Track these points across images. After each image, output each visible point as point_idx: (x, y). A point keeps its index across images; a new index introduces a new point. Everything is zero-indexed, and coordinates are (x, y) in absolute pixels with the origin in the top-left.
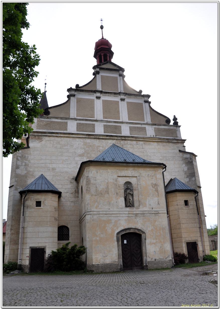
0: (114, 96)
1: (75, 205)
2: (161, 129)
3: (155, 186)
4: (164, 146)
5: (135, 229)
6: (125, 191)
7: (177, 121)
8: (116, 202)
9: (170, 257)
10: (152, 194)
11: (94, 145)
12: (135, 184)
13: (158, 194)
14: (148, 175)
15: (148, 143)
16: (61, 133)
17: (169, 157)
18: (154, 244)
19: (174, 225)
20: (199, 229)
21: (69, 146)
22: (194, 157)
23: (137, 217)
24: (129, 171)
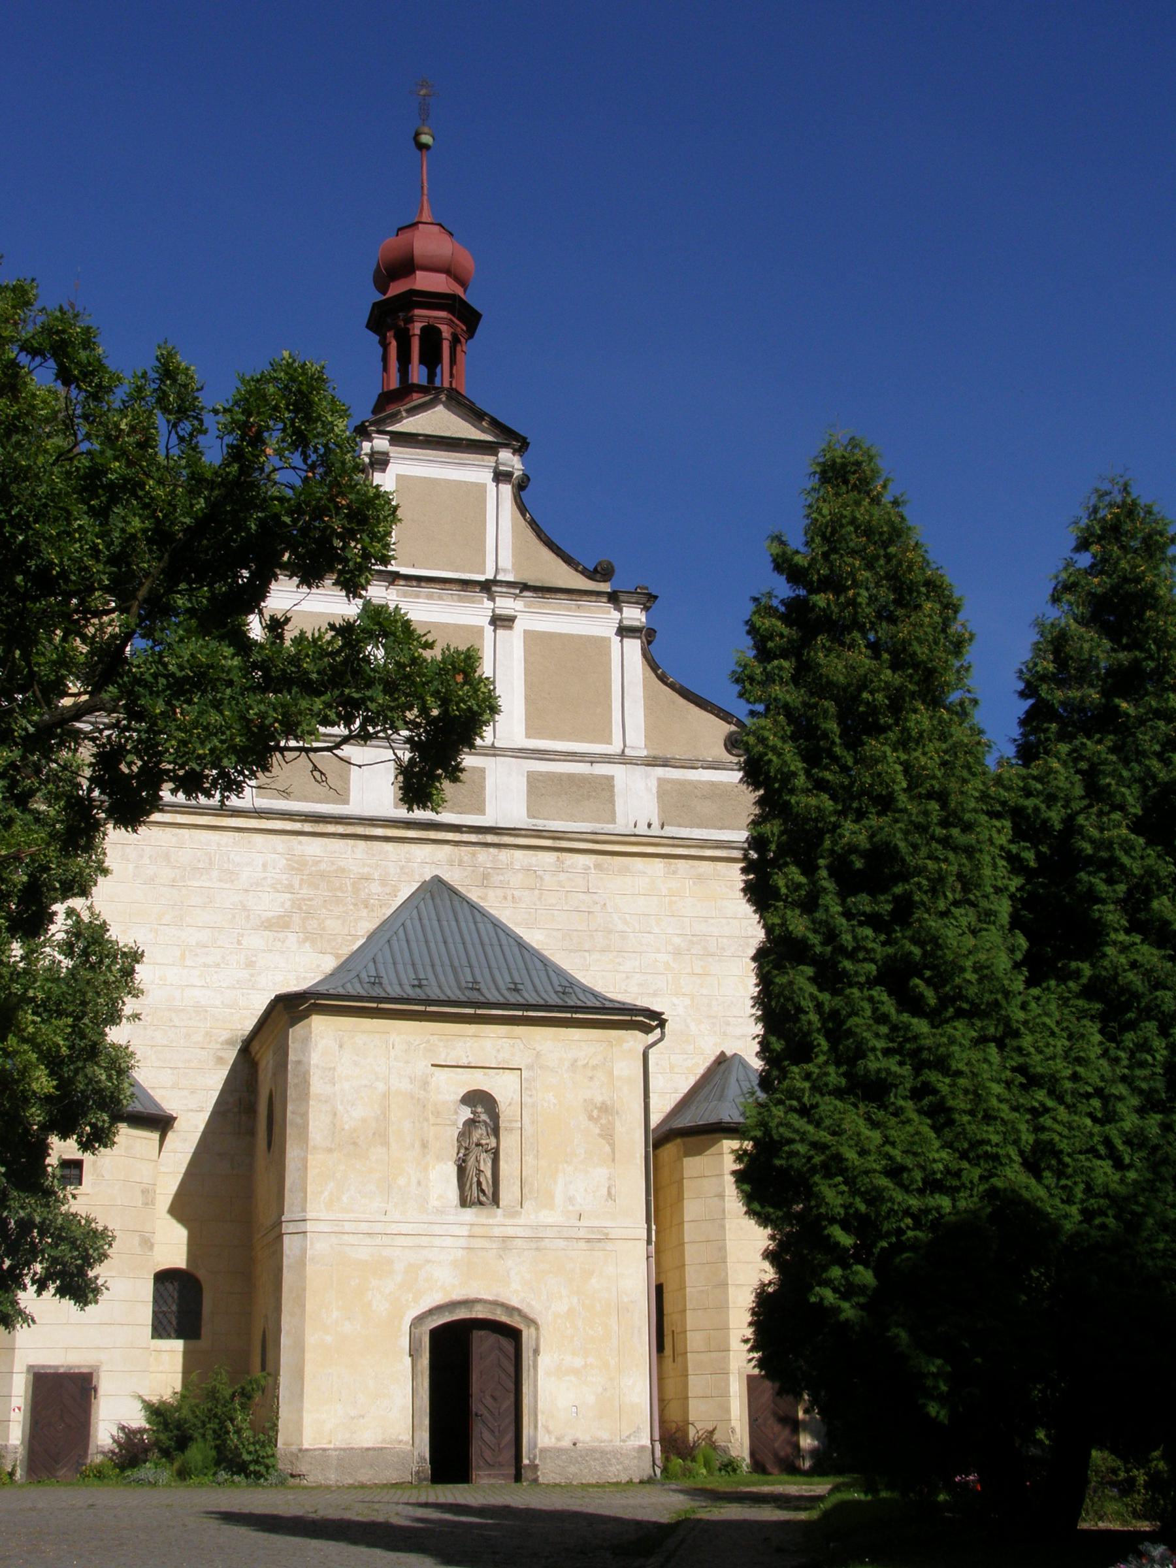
2: (695, 785)
3: (603, 1112)
5: (496, 1303)
8: (419, 1183)
11: (343, 870)
12: (510, 1104)
14: (576, 1061)
21: (215, 874)
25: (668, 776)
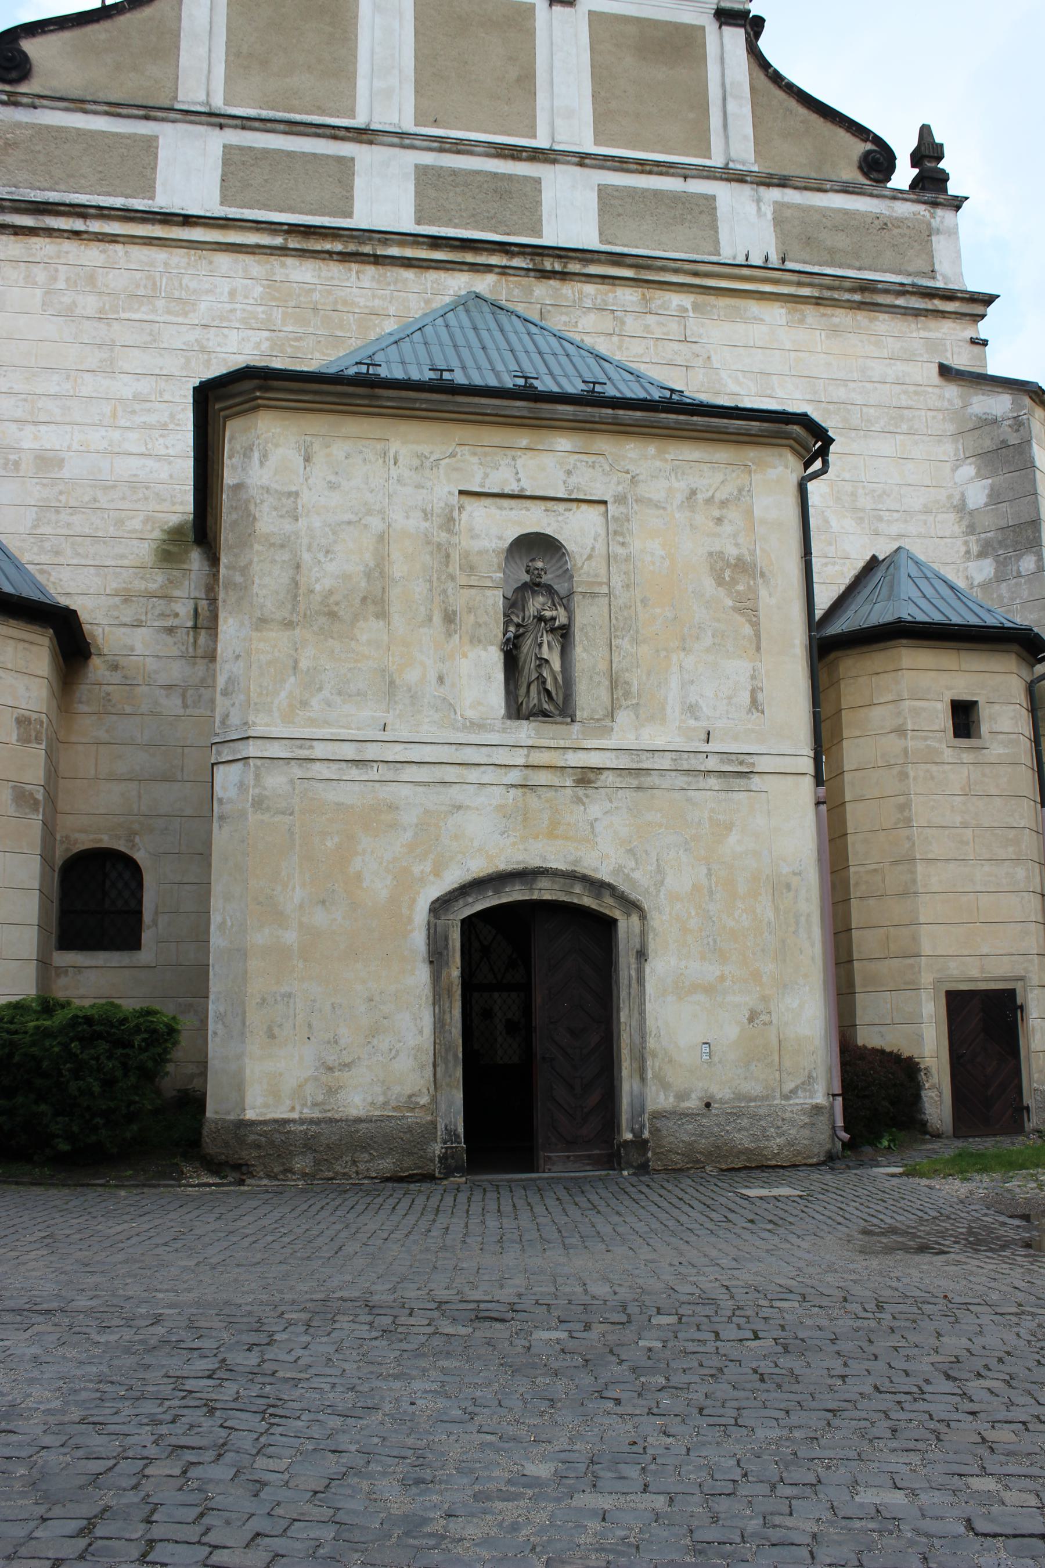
1: (188, 712)
4: (835, 331)
5: (572, 876)
6: (514, 604)
7: (941, 165)
8: (441, 679)
9: (806, 1083)
10: (710, 634)
11: (345, 303)
12: (590, 557)
13: (758, 635)
14: (693, 493)
15: (723, 302)
16: (103, 213)
17: (865, 410)
18: (709, 990)
21: (160, 303)
23: (590, 791)
24: (548, 460)
25: (786, 199)
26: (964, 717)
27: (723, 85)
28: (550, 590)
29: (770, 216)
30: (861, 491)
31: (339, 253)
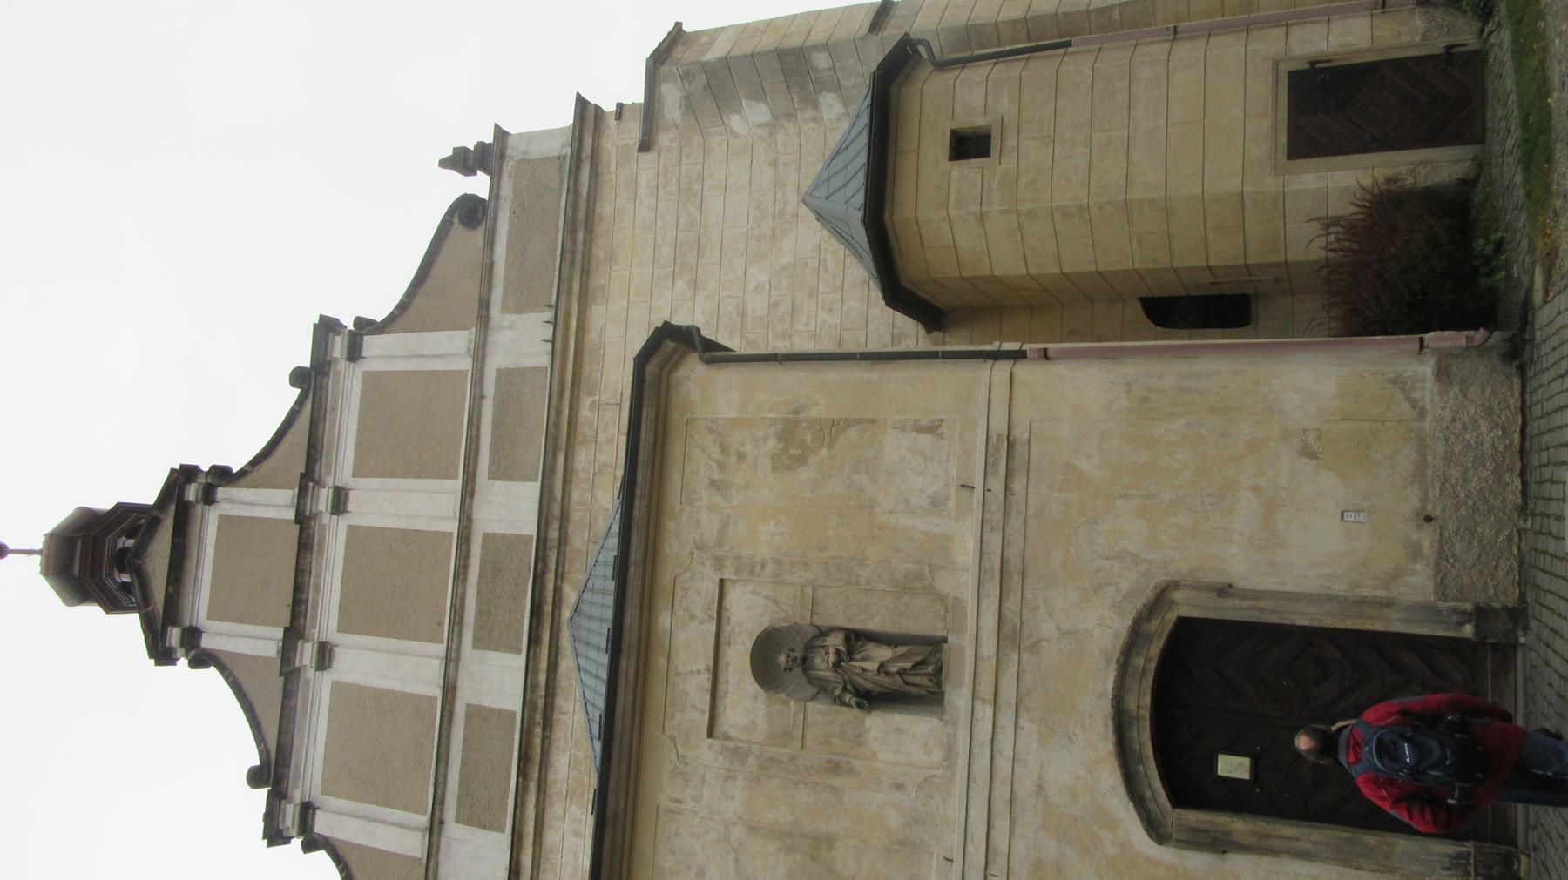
0: (321, 553)
4: (611, 257)
6: (822, 689)
8: (899, 787)
9: (1404, 379)
10: (856, 476)
12: (776, 602)
13: (858, 422)
14: (713, 483)
15: (587, 368)
19: (1135, 246)
20: (1187, 45)
22: (678, 52)
24: (681, 637)
26: (969, 145)
27: (409, 357)
28: (809, 647)
29: (514, 317)
30: (756, 232)
31: (544, 730)
